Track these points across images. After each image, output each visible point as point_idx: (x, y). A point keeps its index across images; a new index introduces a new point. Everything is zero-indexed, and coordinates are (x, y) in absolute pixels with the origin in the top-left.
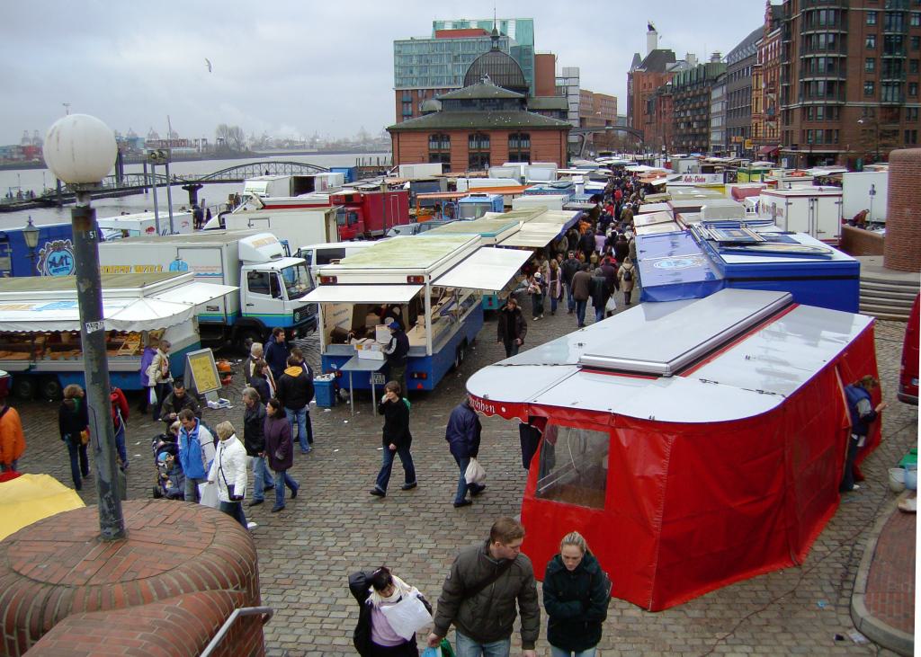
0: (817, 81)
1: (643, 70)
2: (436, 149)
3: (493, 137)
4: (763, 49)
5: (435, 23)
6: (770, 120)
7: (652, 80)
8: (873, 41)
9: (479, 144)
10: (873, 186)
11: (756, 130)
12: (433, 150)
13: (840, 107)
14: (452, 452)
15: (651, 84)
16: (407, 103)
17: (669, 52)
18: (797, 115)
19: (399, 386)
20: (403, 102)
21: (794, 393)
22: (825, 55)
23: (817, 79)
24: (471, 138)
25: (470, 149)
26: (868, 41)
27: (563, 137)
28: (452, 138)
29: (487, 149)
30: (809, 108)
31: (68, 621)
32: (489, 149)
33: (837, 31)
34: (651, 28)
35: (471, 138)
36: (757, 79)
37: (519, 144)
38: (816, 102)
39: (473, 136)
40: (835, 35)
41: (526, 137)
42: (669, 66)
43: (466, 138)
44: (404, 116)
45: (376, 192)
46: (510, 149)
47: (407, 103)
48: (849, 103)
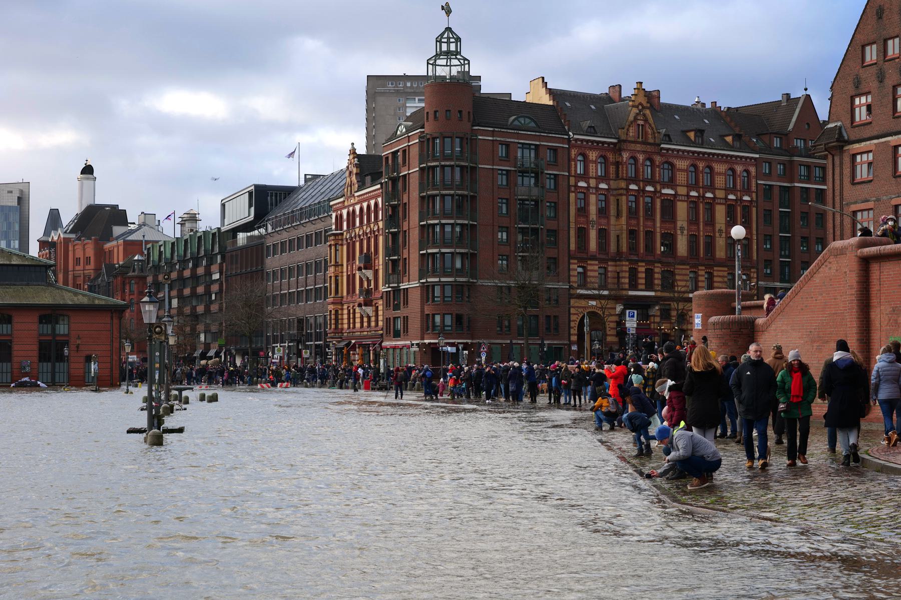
0: (445, 253)
1: (73, 236)
2: (47, 335)
4: (345, 212)
6: (366, 305)
7: (90, 252)
8: (505, 235)
10: (353, 144)
11: (337, 319)
13: (471, 286)
17: (115, 207)
18: (415, 299)
22: (452, 250)
23: (443, 250)
26: (500, 234)
27: (116, 321)
28: (15, 319)
29: (7, 335)
30: (433, 286)
31: (885, 32)
32: (11, 335)
33: (466, 222)
34: (88, 170)
36: (336, 250)
37: (54, 329)
38: (443, 279)
40: (462, 225)
42: (117, 230)
43: (36, 319)
46: (40, 335)
48: (480, 282)
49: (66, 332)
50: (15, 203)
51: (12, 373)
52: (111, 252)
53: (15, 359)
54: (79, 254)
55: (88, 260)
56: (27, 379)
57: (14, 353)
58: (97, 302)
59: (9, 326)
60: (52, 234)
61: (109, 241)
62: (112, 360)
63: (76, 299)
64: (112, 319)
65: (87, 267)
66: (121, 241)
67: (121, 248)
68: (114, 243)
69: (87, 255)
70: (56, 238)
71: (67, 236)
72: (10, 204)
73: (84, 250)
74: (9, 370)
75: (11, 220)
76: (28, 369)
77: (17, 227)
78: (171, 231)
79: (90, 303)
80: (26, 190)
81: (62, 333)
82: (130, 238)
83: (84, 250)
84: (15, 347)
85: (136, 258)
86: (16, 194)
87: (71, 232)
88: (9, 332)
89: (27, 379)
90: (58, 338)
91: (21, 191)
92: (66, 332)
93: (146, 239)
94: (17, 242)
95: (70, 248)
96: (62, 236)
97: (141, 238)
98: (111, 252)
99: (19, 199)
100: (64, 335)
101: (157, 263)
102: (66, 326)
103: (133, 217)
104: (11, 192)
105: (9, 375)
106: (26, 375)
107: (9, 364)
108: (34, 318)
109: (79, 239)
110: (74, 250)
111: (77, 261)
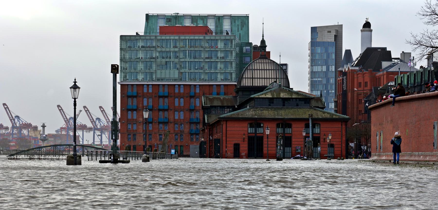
1: (357, 68)
2: (253, 133)
3: (294, 125)
5: (314, 30)
7: (367, 78)
9: (284, 131)
12: (250, 133)
14: (282, 160)
15: (366, 83)
16: (132, 97)
17: (384, 49)
19: (249, 122)
20: (129, 97)
21: (121, 93)
24: (278, 126)
25: (249, 133)
27: (344, 126)
32: (291, 134)
34: (367, 25)
35: (278, 126)
37: (256, 131)
39: (279, 124)
41: (290, 126)
42: (385, 64)
44: (128, 110)
45: (189, 208)
47: (132, 97)
49: (319, 132)
50: (333, 40)
51: (292, 152)
52: (379, 78)
53: (293, 146)
54: (361, 80)
55: (366, 83)
56: (299, 156)
57: (293, 143)
58: (334, 117)
59: (290, 129)
60: (345, 67)
61: (379, 71)
62: (342, 146)
63: (324, 115)
64: (342, 125)
65: (366, 88)
66: (385, 72)
67: (385, 76)
68: (381, 73)
69: (365, 81)
70: (347, 70)
71: (353, 68)
72: (329, 40)
73: (364, 77)
74: (290, 151)
75: (329, 52)
76: (299, 151)
77: (334, 57)
78: (421, 63)
79: (331, 117)
80: (339, 30)
81: (316, 132)
82: (391, 70)
83: (364, 77)
84: (293, 140)
85: (389, 84)
86: (333, 33)
87: (356, 65)
88: (290, 132)
89: (299, 156)
90: (286, 135)
91: (337, 31)
92: (319, 132)
93: (401, 70)
94: (334, 67)
95: (355, 76)
96: (350, 69)
97: (398, 70)
98: (379, 78)
99: (336, 36)
100: (317, 134)
101: (419, 84)
102: (319, 129)
103: (395, 54)
104: (330, 32)
105: (290, 153)
106: (298, 153)
107: (290, 148)
108: (274, 125)
109: (360, 70)
110: (357, 78)
111: (359, 85)
